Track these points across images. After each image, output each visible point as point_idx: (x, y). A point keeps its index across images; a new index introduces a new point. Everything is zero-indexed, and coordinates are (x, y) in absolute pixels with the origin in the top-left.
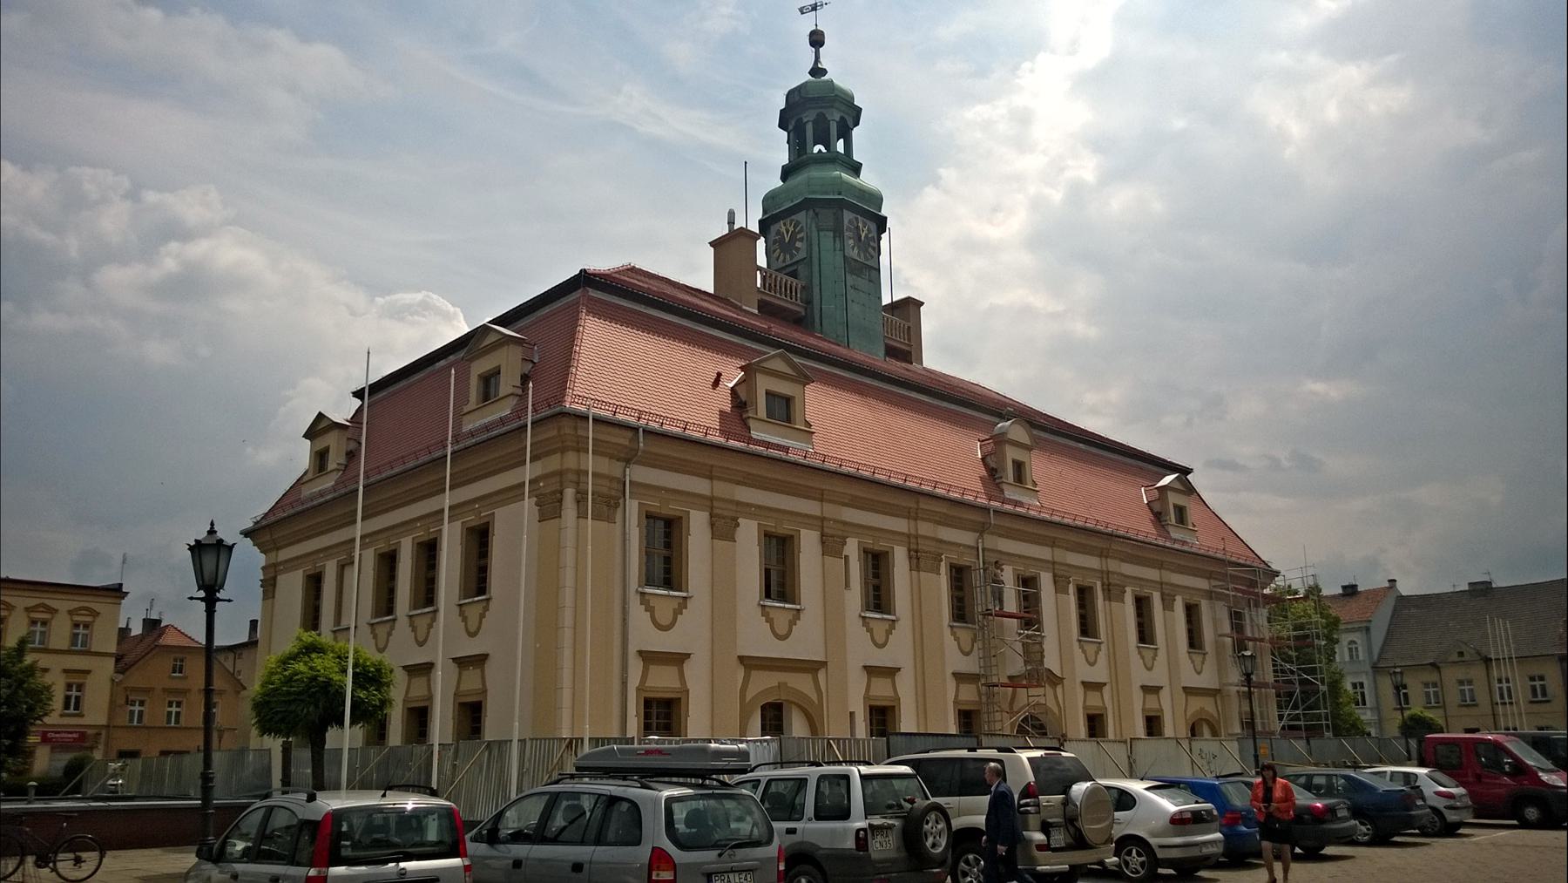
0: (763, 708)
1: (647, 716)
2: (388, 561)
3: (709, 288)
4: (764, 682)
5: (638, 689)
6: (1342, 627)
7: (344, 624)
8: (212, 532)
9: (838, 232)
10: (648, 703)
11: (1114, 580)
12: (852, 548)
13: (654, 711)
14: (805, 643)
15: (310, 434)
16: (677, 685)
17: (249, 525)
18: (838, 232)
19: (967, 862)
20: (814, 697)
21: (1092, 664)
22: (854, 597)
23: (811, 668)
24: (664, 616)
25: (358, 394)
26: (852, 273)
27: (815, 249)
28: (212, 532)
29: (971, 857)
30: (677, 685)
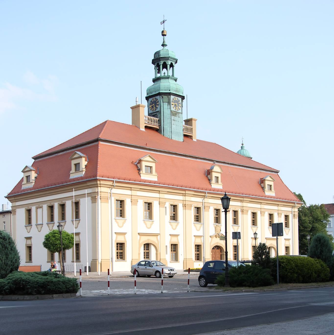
0: (144, 245)
1: (117, 247)
2: (51, 208)
3: (131, 124)
4: (145, 239)
5: (115, 241)
6: (224, 195)
7: (40, 222)
8: (255, 232)
9: (169, 103)
10: (117, 244)
11: (206, 205)
12: (168, 205)
13: (119, 246)
14: (154, 229)
15: (23, 171)
16: (177, 241)
17: (6, 195)
18: (169, 103)
19: (202, 279)
20: (157, 242)
21: (39, 231)
22: (168, 217)
23: (156, 235)
24: (174, 227)
25: (33, 158)
26: (173, 115)
27: (162, 108)
28: (255, 232)
29: (203, 279)
30: (177, 241)
